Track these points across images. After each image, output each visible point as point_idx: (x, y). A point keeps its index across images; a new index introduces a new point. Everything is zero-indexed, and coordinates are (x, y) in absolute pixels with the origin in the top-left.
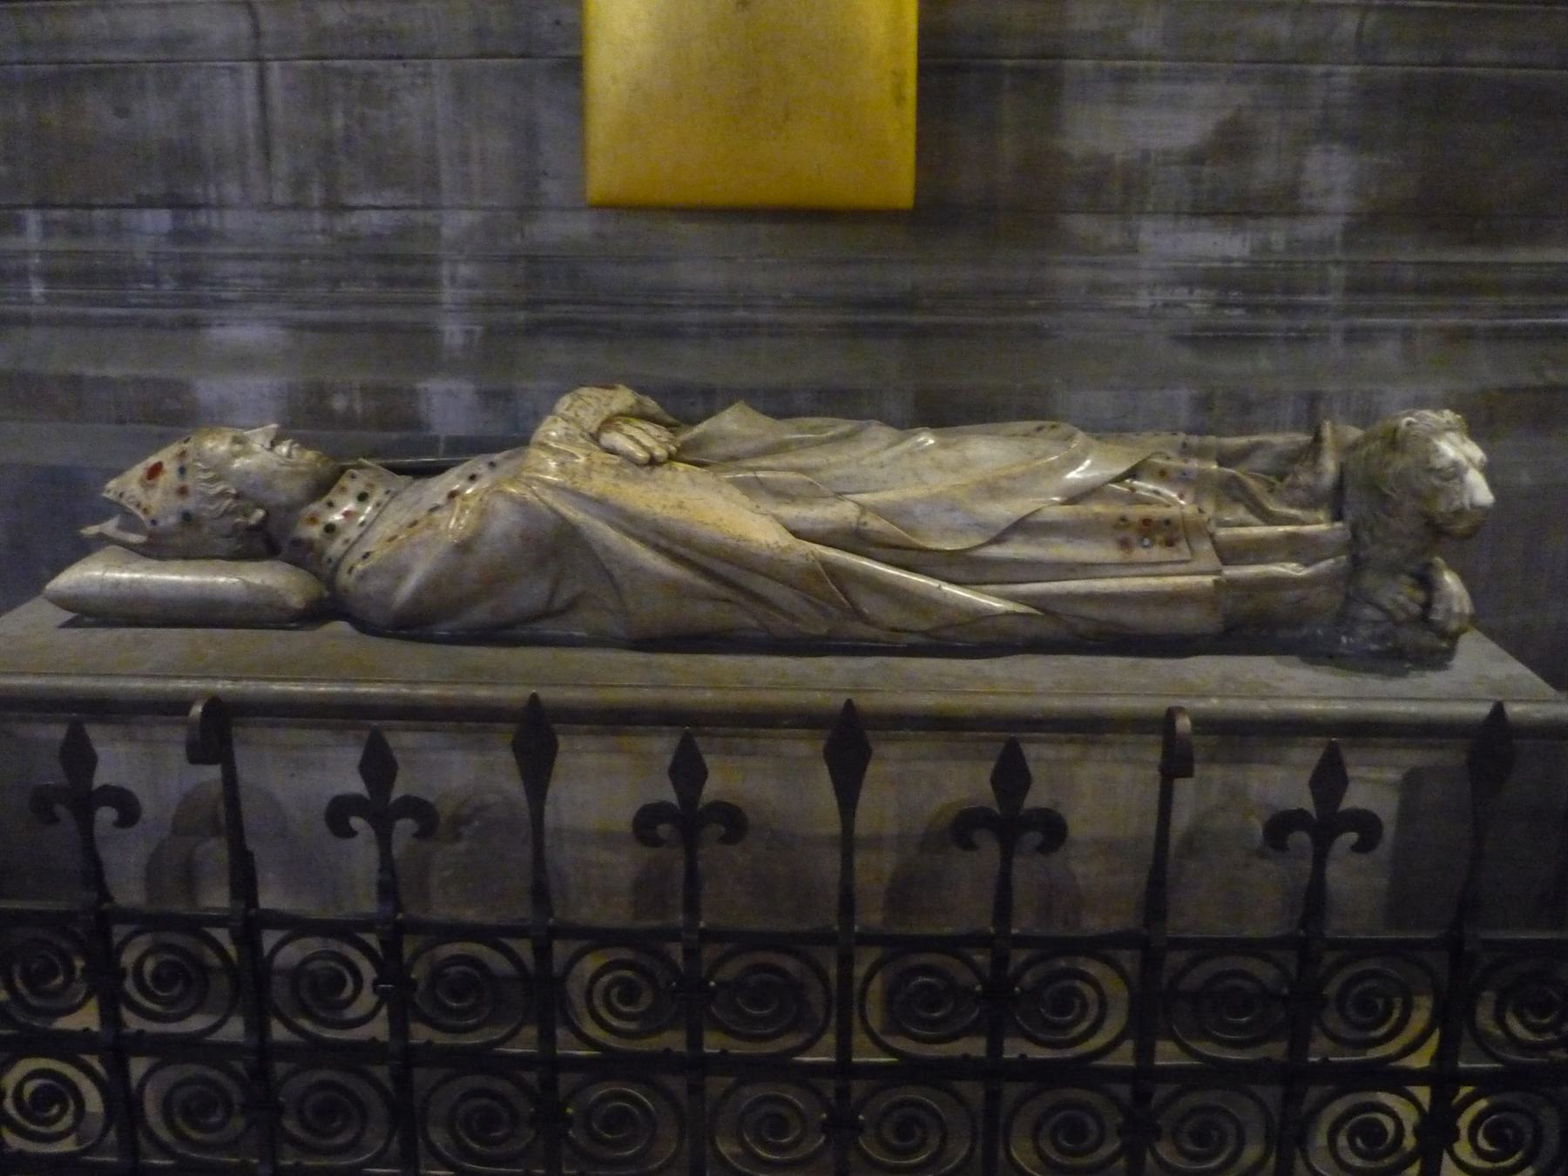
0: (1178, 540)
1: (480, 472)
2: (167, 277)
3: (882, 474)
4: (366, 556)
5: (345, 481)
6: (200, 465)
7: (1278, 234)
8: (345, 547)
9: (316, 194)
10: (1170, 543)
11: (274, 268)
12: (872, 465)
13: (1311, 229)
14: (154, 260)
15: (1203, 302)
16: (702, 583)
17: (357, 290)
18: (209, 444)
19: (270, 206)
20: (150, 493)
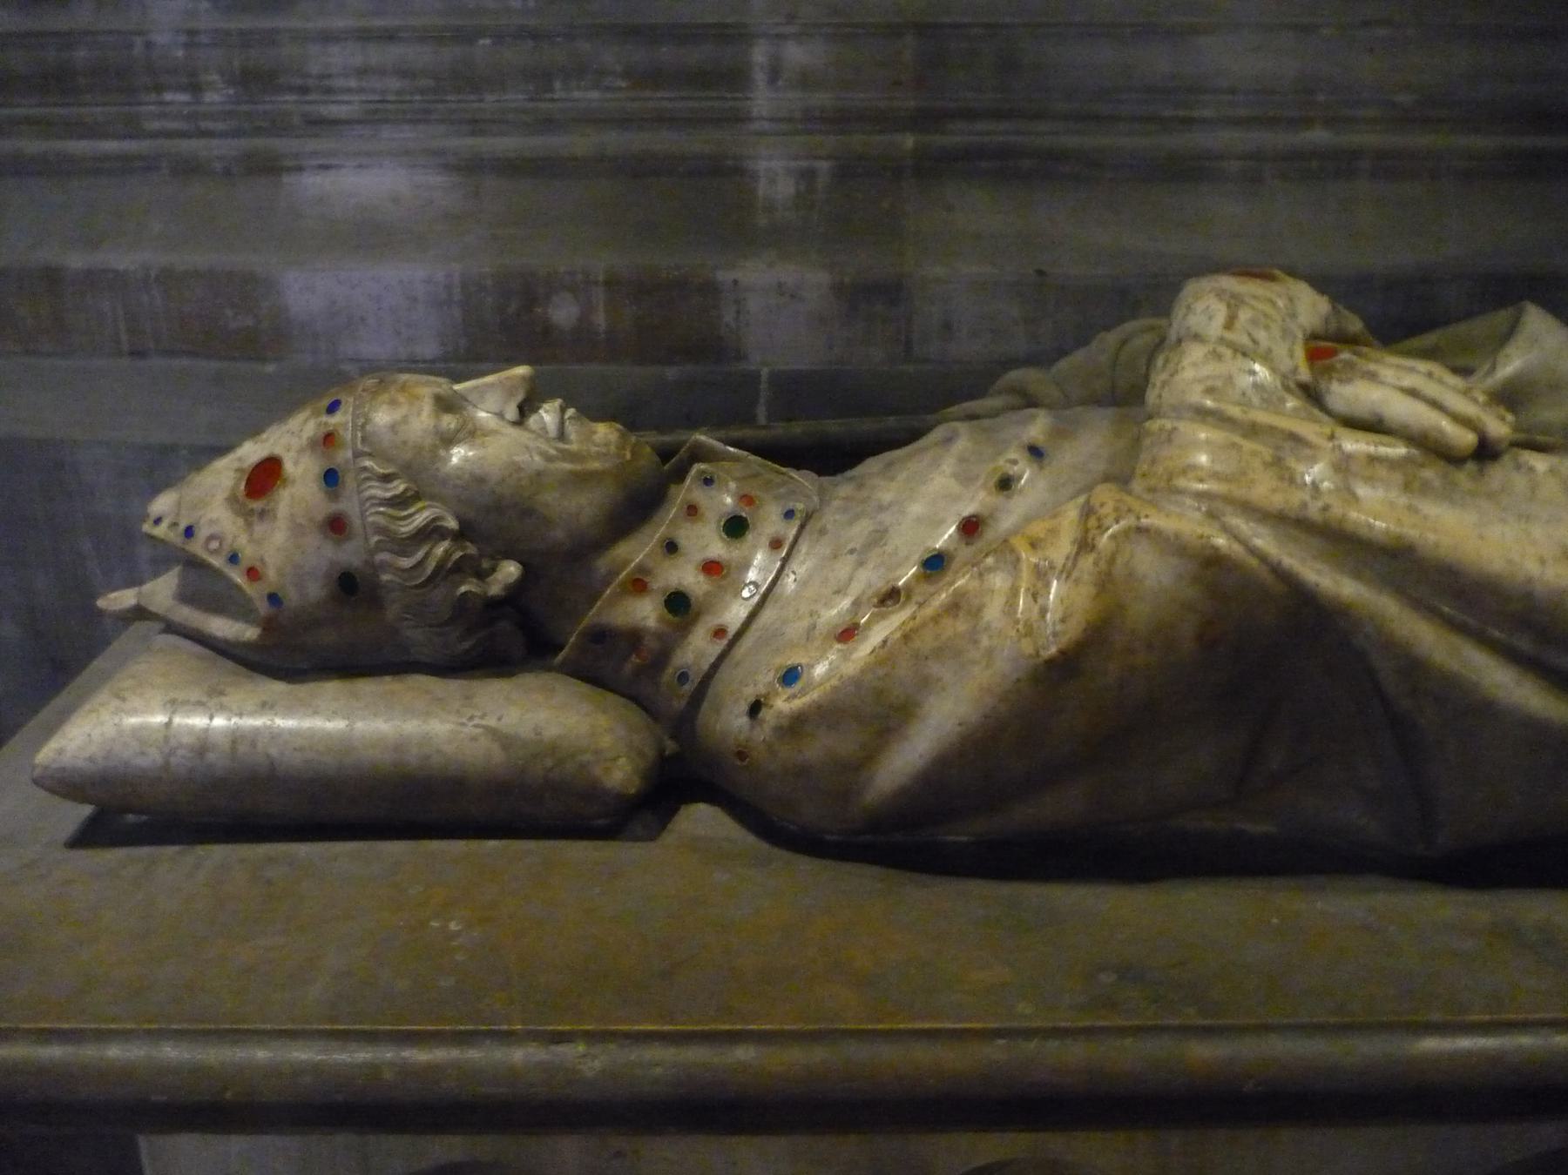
2: (215, 77)
5: (688, 490)
6: (368, 463)
8: (720, 646)
11: (419, 55)
14: (187, 46)
18: (382, 417)
20: (259, 529)
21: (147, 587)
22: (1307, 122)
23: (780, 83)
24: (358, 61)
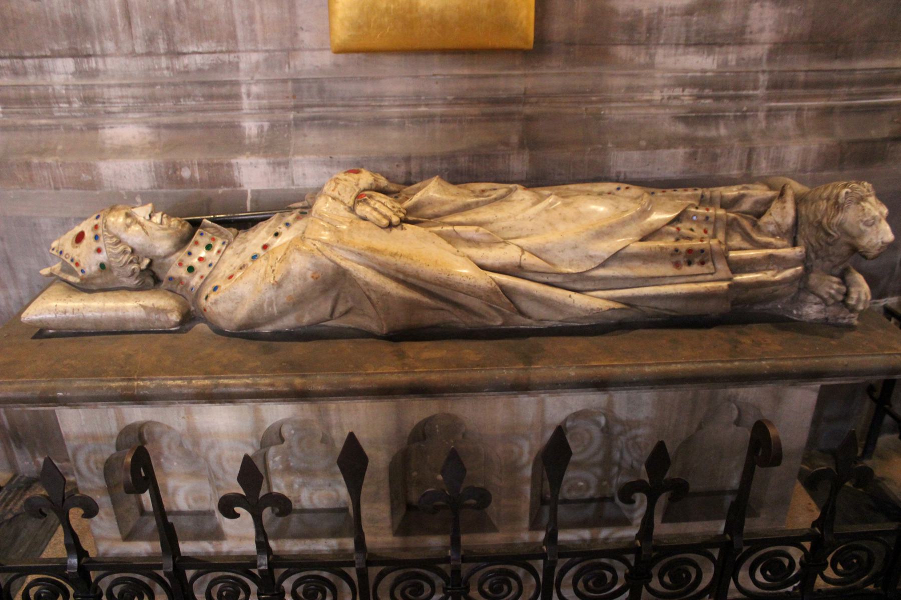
0: (708, 260)
1: (281, 230)
2: (76, 99)
3: (529, 225)
4: (215, 289)
7: (732, 56)
8: (202, 280)
9: (162, 46)
10: (702, 263)
11: (137, 91)
12: (524, 219)
13: (751, 52)
14: (66, 89)
15: (690, 96)
16: (426, 300)
17: (191, 103)
19: (133, 54)
21: (53, 267)
22: (420, 105)
23: (251, 98)
24: (120, 94)
